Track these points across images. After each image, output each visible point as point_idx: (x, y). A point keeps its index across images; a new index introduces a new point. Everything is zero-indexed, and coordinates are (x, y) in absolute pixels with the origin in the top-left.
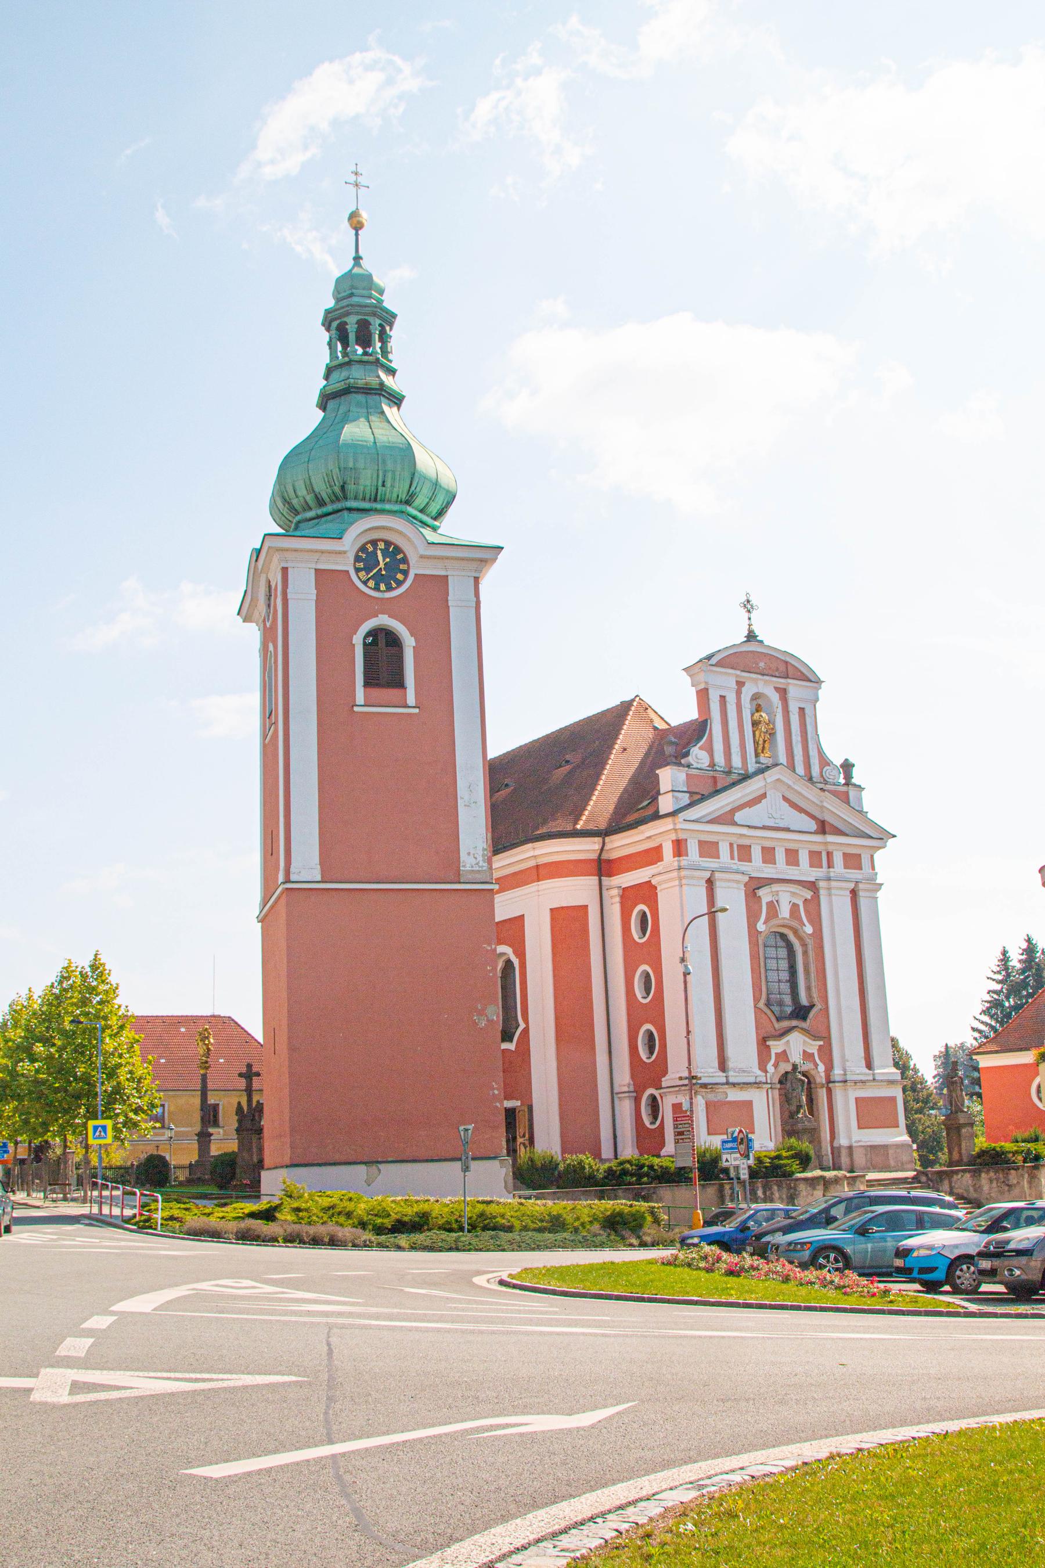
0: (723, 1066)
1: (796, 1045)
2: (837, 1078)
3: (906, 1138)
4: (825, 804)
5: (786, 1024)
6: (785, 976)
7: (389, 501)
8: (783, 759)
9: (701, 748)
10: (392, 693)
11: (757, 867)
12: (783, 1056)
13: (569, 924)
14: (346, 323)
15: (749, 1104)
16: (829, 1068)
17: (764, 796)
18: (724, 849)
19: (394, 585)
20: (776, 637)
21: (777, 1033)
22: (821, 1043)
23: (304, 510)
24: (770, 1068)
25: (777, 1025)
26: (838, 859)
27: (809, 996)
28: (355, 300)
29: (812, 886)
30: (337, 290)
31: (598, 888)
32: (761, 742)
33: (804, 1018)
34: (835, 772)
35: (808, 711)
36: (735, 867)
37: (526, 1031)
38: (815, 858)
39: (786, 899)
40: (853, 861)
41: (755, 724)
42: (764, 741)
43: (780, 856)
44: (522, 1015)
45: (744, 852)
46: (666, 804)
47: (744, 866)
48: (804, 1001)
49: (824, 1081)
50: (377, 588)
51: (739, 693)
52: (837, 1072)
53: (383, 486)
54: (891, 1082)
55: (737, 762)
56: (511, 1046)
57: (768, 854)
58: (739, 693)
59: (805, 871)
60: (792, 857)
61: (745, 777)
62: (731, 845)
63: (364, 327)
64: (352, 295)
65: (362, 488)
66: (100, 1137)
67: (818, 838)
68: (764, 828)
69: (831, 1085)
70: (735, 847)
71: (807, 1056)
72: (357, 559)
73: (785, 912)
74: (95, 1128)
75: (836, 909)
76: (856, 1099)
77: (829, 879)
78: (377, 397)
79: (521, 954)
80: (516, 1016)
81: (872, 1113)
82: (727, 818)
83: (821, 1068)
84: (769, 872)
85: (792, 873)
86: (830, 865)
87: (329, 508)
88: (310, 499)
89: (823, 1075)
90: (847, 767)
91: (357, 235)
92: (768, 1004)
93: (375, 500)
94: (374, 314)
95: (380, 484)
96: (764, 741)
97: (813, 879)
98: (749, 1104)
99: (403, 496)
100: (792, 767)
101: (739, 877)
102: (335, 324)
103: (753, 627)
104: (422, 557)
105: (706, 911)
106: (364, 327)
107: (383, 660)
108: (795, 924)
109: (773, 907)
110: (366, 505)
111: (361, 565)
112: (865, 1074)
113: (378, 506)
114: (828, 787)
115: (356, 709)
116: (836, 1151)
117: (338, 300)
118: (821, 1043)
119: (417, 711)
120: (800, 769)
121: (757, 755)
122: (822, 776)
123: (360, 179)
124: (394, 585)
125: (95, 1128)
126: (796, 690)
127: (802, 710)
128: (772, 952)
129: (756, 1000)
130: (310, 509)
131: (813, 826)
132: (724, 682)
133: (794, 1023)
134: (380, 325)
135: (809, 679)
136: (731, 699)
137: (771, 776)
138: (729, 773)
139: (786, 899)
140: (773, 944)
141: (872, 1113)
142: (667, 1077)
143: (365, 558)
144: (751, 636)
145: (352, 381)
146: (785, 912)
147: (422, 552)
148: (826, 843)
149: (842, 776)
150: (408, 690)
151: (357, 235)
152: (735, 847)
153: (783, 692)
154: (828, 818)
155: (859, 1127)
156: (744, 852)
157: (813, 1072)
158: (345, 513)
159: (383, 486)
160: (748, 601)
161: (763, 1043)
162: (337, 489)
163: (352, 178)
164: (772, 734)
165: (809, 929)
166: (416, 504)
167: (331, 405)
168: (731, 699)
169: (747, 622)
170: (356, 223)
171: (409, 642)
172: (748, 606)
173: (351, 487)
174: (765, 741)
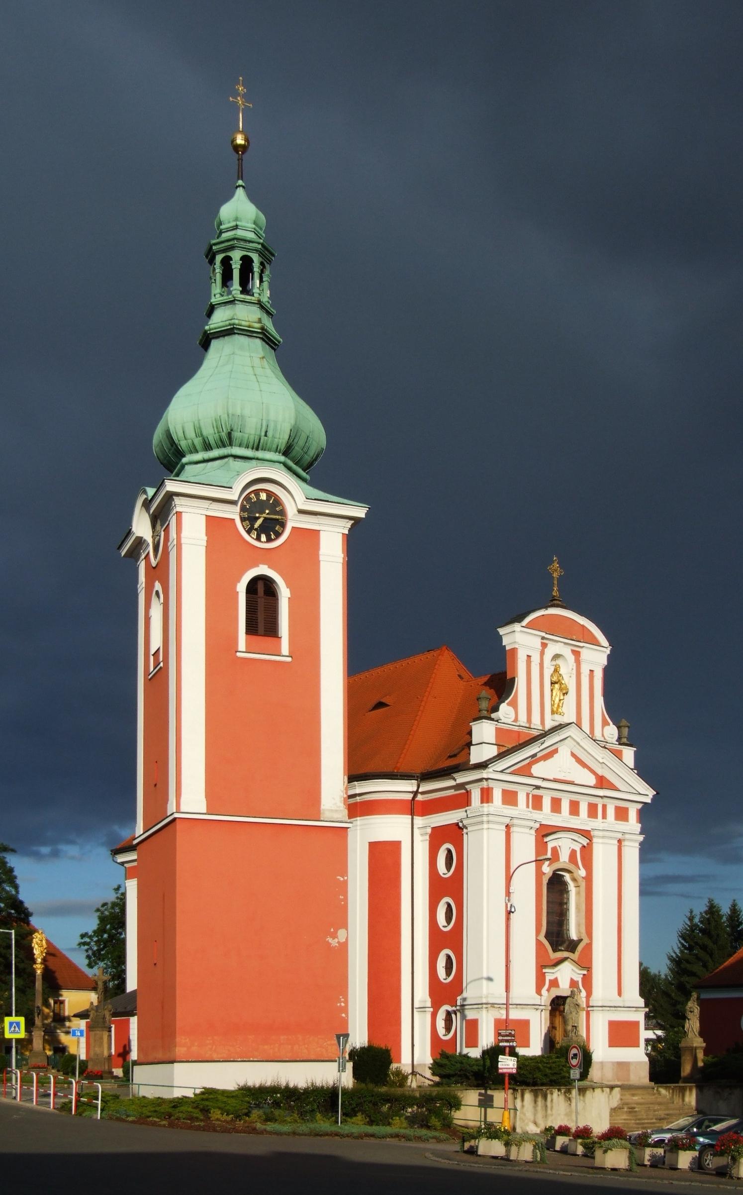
1: (566, 974)
7: (269, 450)
10: (270, 640)
11: (546, 816)
12: (554, 983)
16: (589, 994)
18: (522, 798)
19: (273, 537)
21: (553, 963)
23: (191, 452)
26: (611, 812)
29: (586, 834)
31: (410, 826)
38: (592, 811)
39: (565, 845)
45: (537, 803)
46: (477, 755)
51: (542, 653)
53: (266, 435)
57: (556, 805)
58: (542, 653)
59: (582, 821)
60: (574, 808)
62: (528, 795)
64: (236, 227)
65: (246, 436)
66: (14, 1032)
68: (555, 781)
73: (564, 857)
74: (11, 1024)
86: (604, 816)
87: (215, 453)
88: (198, 442)
89: (584, 1000)
93: (257, 449)
95: (263, 434)
101: (532, 824)
104: (301, 512)
105: (534, 859)
108: (571, 867)
110: (249, 453)
113: (260, 454)
115: (239, 654)
119: (289, 659)
120: (586, 726)
122: (603, 735)
124: (273, 537)
125: (11, 1024)
129: (538, 932)
130: (197, 452)
131: (592, 780)
136: (536, 659)
139: (565, 845)
145: (236, 322)
146: (564, 857)
150: (283, 639)
153: (577, 654)
158: (231, 459)
159: (266, 435)
162: (224, 435)
165: (582, 872)
168: (536, 659)
171: (284, 593)
173: (236, 435)
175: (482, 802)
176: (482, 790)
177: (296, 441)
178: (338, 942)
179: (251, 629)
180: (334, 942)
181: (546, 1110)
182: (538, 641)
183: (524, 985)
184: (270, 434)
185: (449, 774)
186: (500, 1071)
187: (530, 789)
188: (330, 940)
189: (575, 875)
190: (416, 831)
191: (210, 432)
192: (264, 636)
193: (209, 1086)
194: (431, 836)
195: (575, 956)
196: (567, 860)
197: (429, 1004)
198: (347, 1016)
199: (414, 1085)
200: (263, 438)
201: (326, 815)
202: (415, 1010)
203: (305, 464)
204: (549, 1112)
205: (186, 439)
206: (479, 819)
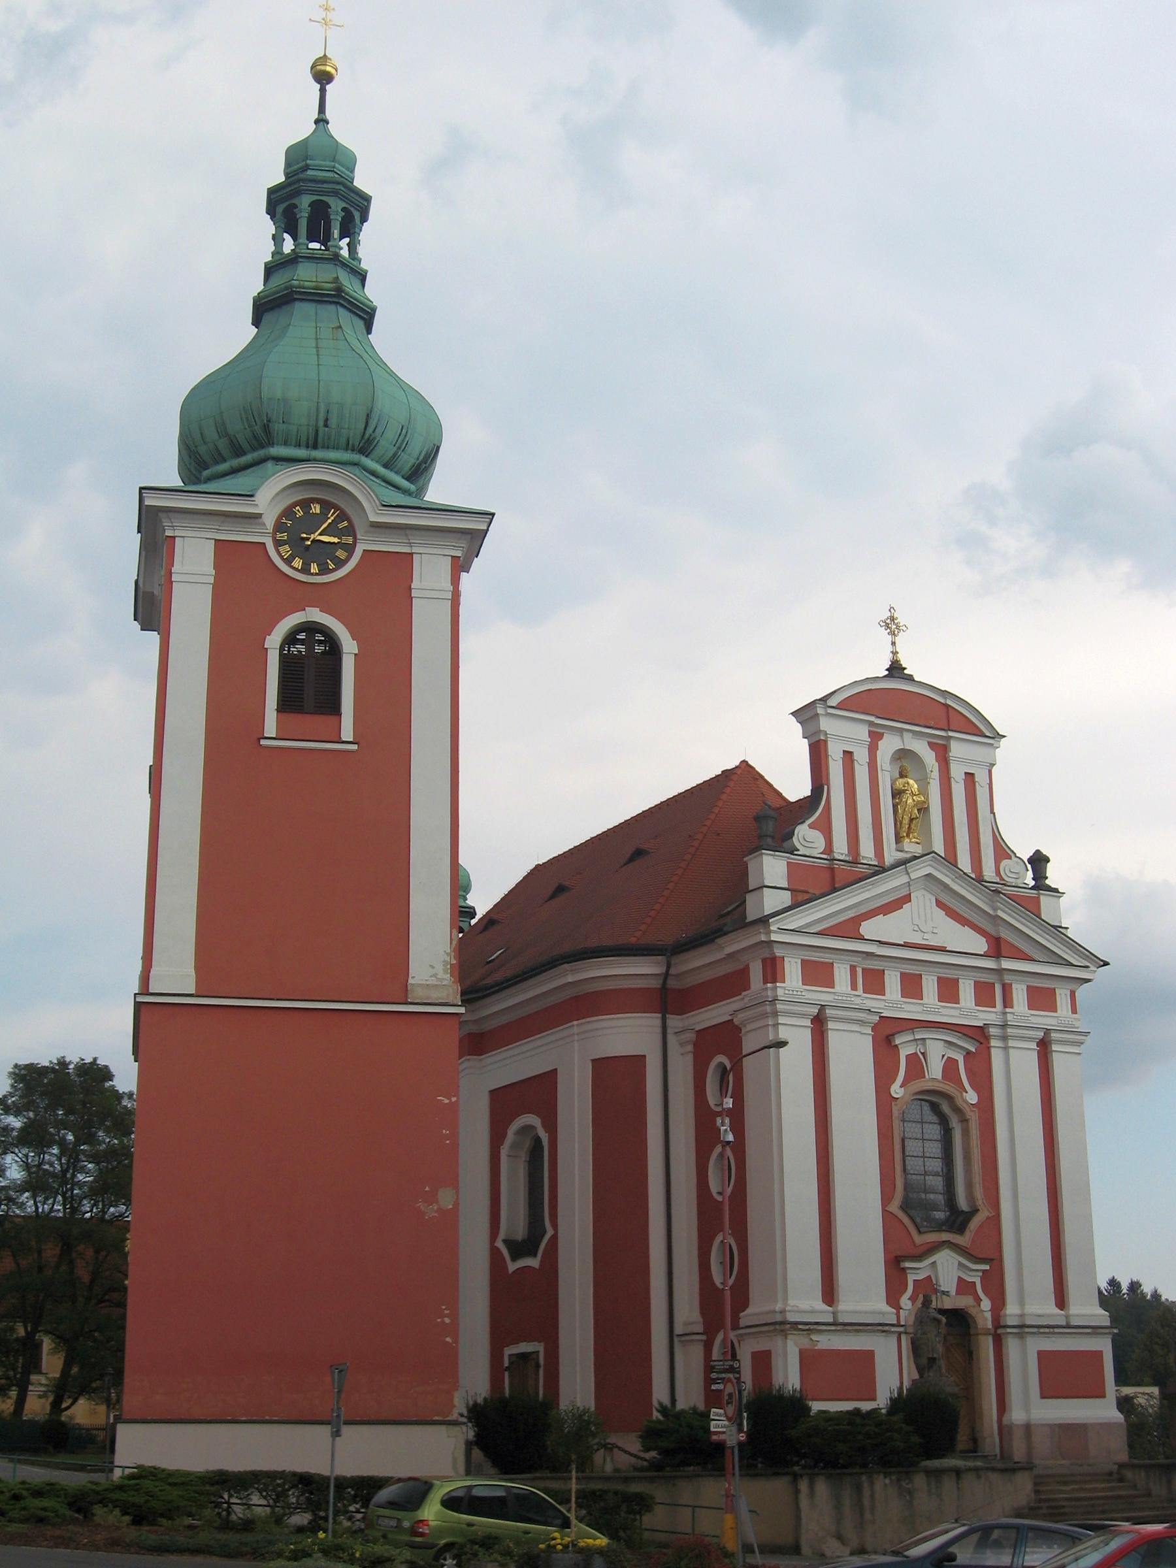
0: (829, 1293)
2: (1011, 1321)
3: (1117, 1416)
4: (1000, 913)
5: (933, 1237)
6: (936, 1165)
7: (336, 447)
8: (939, 847)
9: (810, 826)
10: (321, 722)
11: (892, 1001)
13: (617, 1080)
14: (295, 206)
15: (869, 1356)
16: (999, 1302)
17: (907, 899)
18: (841, 974)
19: (331, 566)
20: (930, 669)
22: (987, 1267)
24: (905, 1301)
25: (919, 1239)
26: (1020, 994)
27: (971, 1198)
28: (309, 172)
29: (980, 1034)
30: (288, 164)
32: (906, 821)
33: (961, 1229)
34: (1019, 868)
35: (981, 778)
36: (858, 1001)
37: (554, 1238)
38: (984, 995)
40: (1042, 998)
41: (897, 794)
42: (910, 822)
43: (930, 986)
44: (550, 1220)
47: (872, 1002)
48: (963, 1203)
49: (990, 1325)
50: (305, 570)
51: (873, 749)
52: (1012, 1310)
53: (326, 425)
54: (1095, 1330)
55: (867, 850)
56: (534, 1262)
58: (873, 749)
59: (967, 1009)
61: (881, 869)
62: (853, 969)
63: (320, 212)
65: (295, 428)
67: (990, 964)
68: (906, 945)
69: (1000, 1331)
70: (859, 971)
71: (964, 1287)
72: (279, 527)
73: (935, 1069)
75: (1015, 1069)
76: (1039, 1353)
77: (1004, 1026)
78: (332, 307)
79: (551, 1125)
80: (543, 1221)
81: (1064, 1375)
82: (849, 929)
83: (986, 1304)
84: (910, 1010)
85: (948, 1014)
86: (1007, 1002)
88: (223, 444)
89: (988, 1315)
90: (1039, 861)
91: (323, 92)
92: (906, 1206)
93: (315, 447)
94: (335, 193)
95: (321, 423)
96: (910, 822)
97: (980, 1024)
98: (869, 1356)
99: (356, 441)
100: (950, 859)
102: (280, 209)
103: (900, 656)
106: (320, 212)
107: (310, 681)
108: (949, 1088)
109: (916, 1065)
110: (301, 453)
111: (285, 536)
112: (883, 1314)
114: (1008, 890)
115: (263, 742)
116: (1004, 1430)
117: (287, 175)
118: (987, 1267)
119: (355, 747)
121: (898, 839)
123: (330, 16)
124: (331, 566)
126: (961, 750)
127: (970, 777)
128: (913, 1130)
129: (886, 1198)
130: (224, 460)
132: (844, 734)
133: (945, 1236)
134: (344, 209)
135: (980, 730)
136: (861, 757)
137: (919, 870)
138: (855, 862)
139: (936, 1054)
140: (918, 1117)
141: (1064, 1375)
142: (748, 1311)
143: (293, 527)
144: (895, 669)
146: (935, 1069)
147: (373, 518)
148: (1000, 971)
149: (1030, 874)
151: (323, 92)
152: (859, 971)
154: (1005, 934)
155: (1043, 1397)
156: (874, 982)
157: (973, 1311)
159: (326, 425)
160: (893, 619)
161: (895, 1266)
162: (258, 429)
163: (319, 15)
164: (923, 809)
165: (972, 1097)
166: (378, 452)
167: (267, 318)
168: (861, 757)
169: (890, 648)
170: (323, 78)
171: (349, 647)
172: (891, 625)
173: (277, 427)
174: (911, 820)
175: (765, 982)
176: (764, 961)
177: (379, 431)
178: (440, 1210)
179: (289, 702)
180: (431, 1211)
181: (862, 1515)
182: (862, 733)
183: (864, 1292)
184: (333, 422)
185: (712, 941)
186: (714, 1437)
187: (856, 960)
188: (421, 1205)
189: (959, 1102)
190: (671, 1039)
191: (236, 427)
192: (315, 713)
193: (148, 1462)
194: (696, 1045)
195: (962, 1240)
196: (940, 1077)
197: (699, 1328)
198: (456, 1341)
199: (609, 1468)
200: (322, 430)
201: (416, 994)
202: (676, 1340)
203: (406, 469)
204: (868, 1516)
205: (205, 443)
206: (759, 1010)
